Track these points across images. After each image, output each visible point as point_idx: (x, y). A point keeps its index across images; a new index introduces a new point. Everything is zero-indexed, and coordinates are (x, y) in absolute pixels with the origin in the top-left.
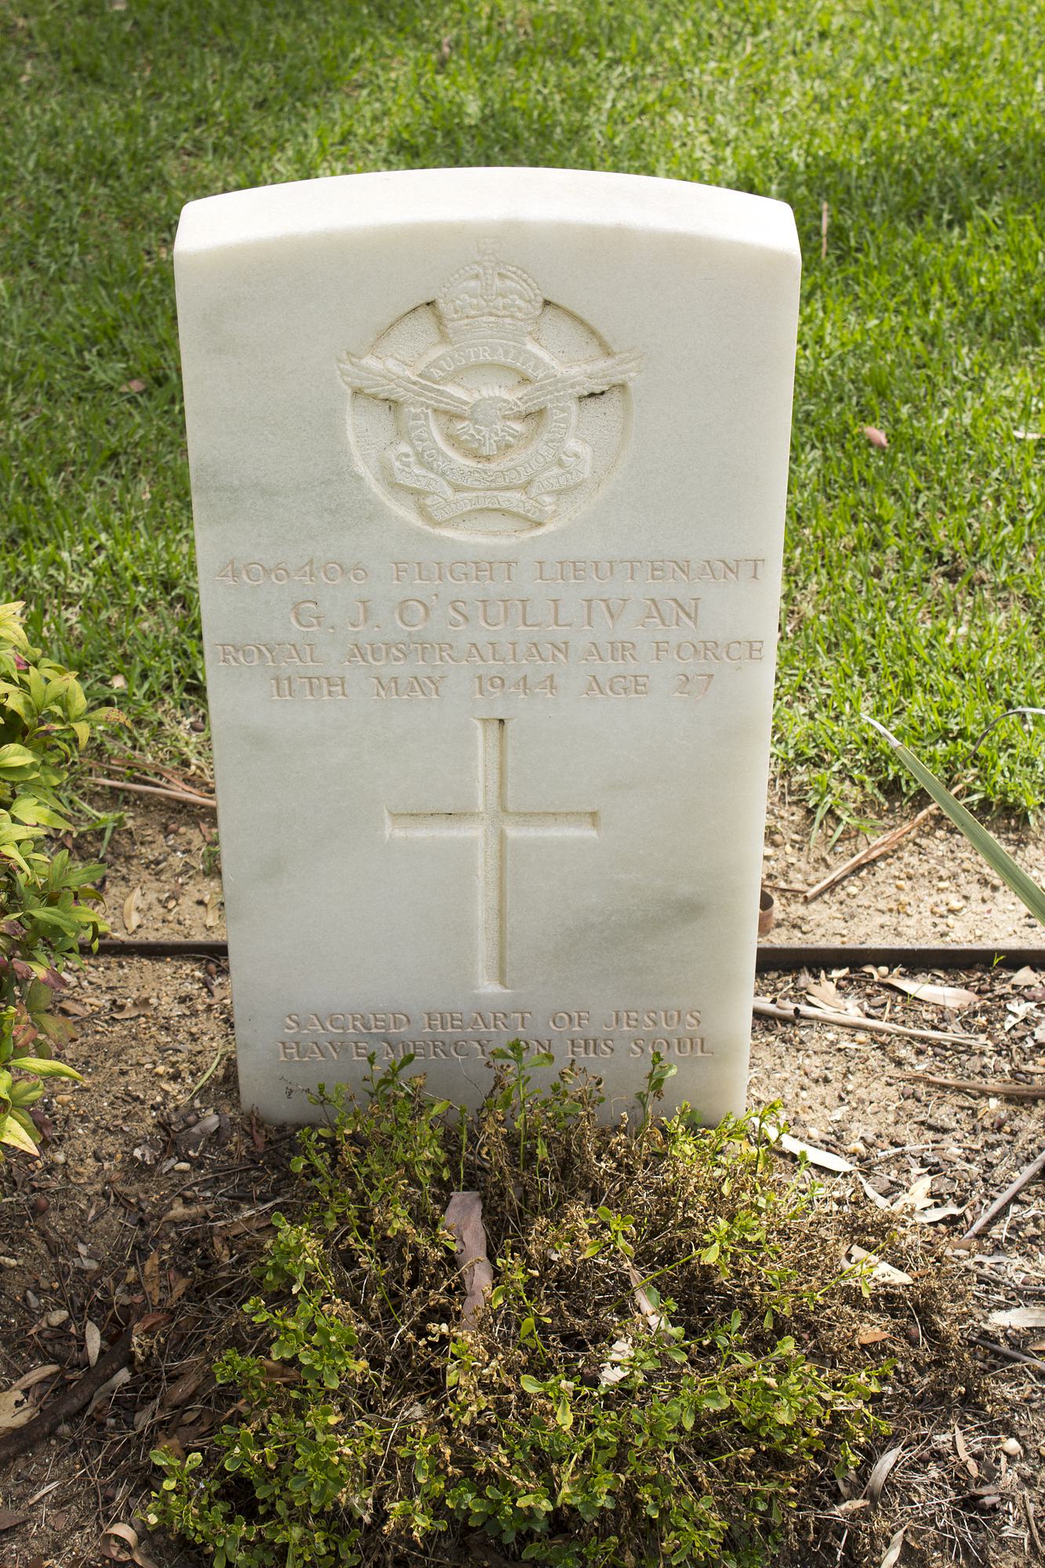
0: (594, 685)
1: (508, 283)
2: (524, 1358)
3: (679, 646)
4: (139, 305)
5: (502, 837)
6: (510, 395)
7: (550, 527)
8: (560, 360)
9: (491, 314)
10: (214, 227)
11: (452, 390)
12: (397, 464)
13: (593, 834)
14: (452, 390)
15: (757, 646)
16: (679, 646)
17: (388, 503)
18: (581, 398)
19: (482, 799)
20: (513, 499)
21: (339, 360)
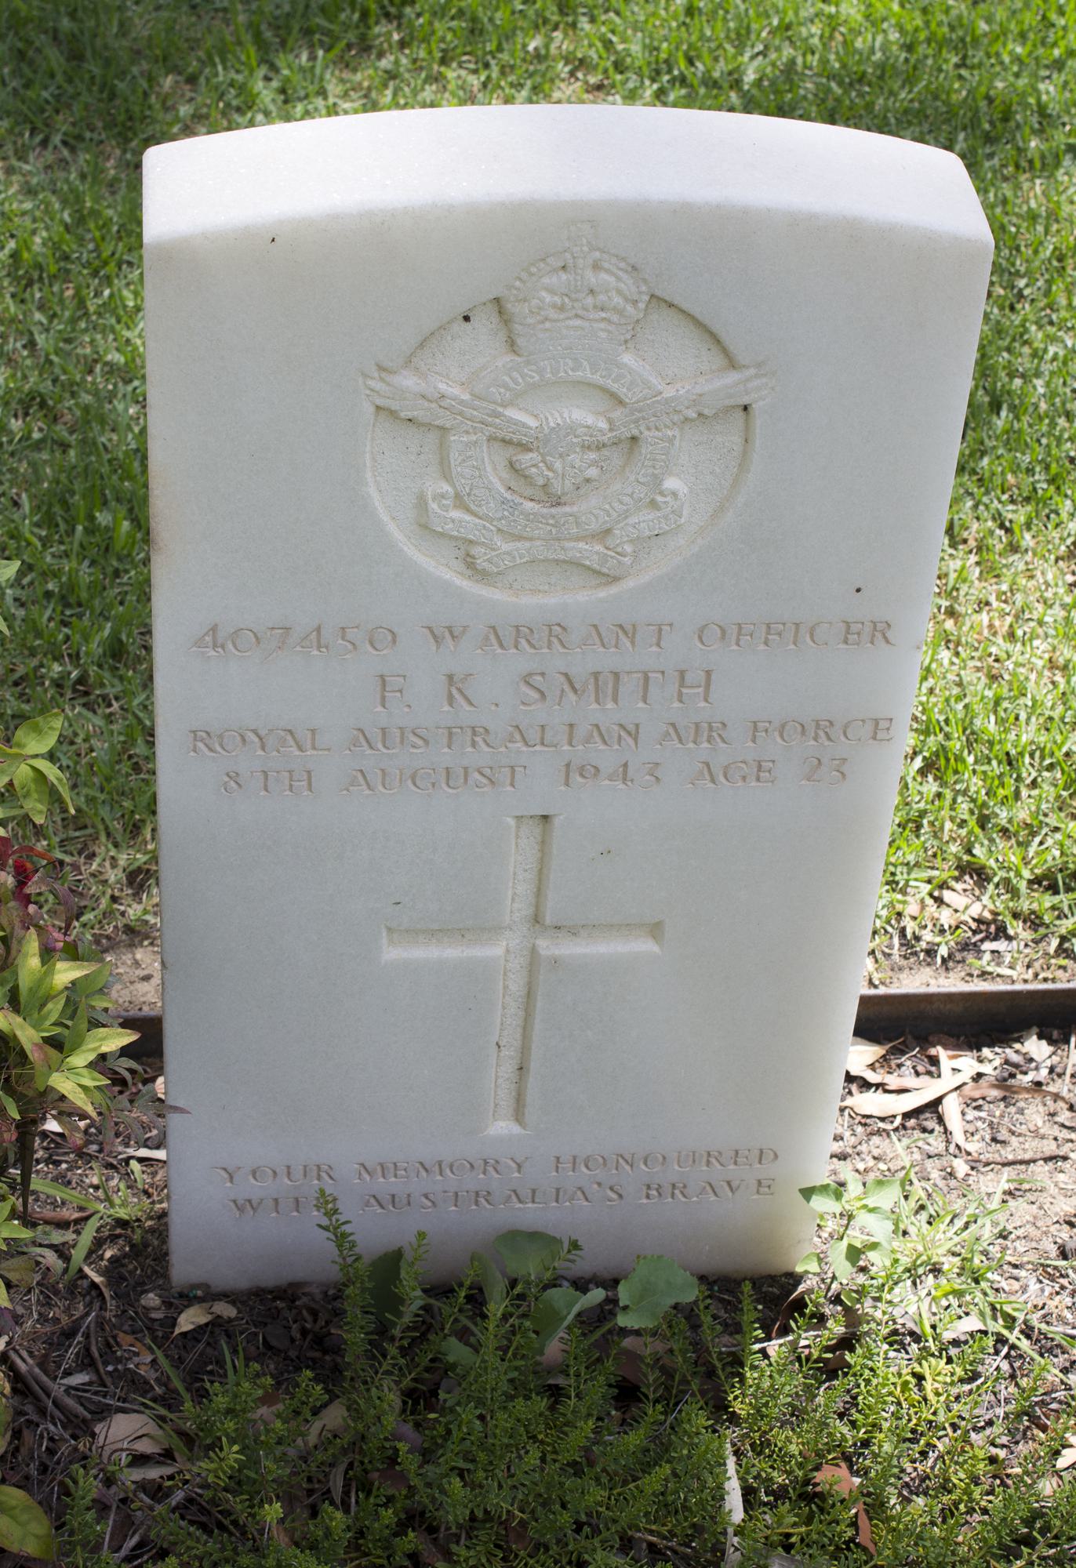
0: (492, 637)
1: (604, 276)
2: (122, 360)
3: (783, 726)
4: (109, 234)
5: (534, 950)
6: (584, 415)
7: (629, 584)
8: (668, 369)
9: (577, 316)
10: (203, 186)
11: (512, 413)
12: (435, 506)
13: (656, 949)
14: (512, 413)
15: (883, 725)
16: (783, 726)
17: (484, 592)
18: (512, 345)
19: (515, 902)
20: (590, 552)
21: (365, 376)
